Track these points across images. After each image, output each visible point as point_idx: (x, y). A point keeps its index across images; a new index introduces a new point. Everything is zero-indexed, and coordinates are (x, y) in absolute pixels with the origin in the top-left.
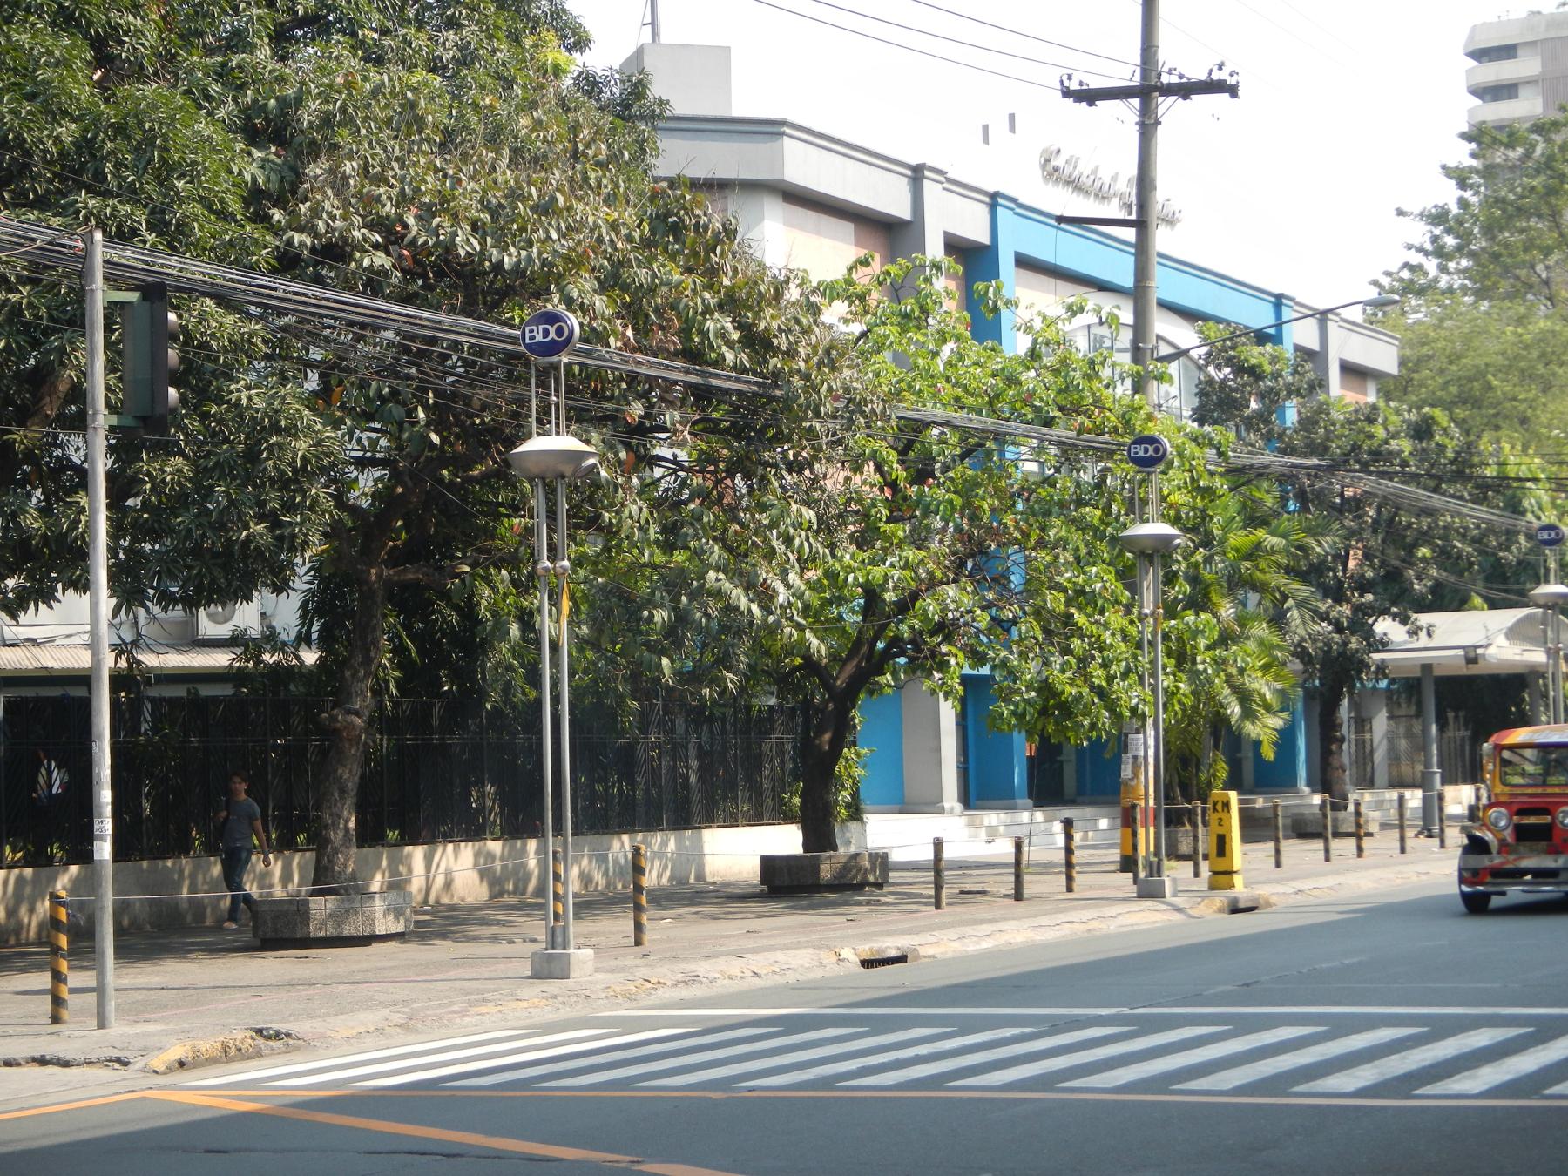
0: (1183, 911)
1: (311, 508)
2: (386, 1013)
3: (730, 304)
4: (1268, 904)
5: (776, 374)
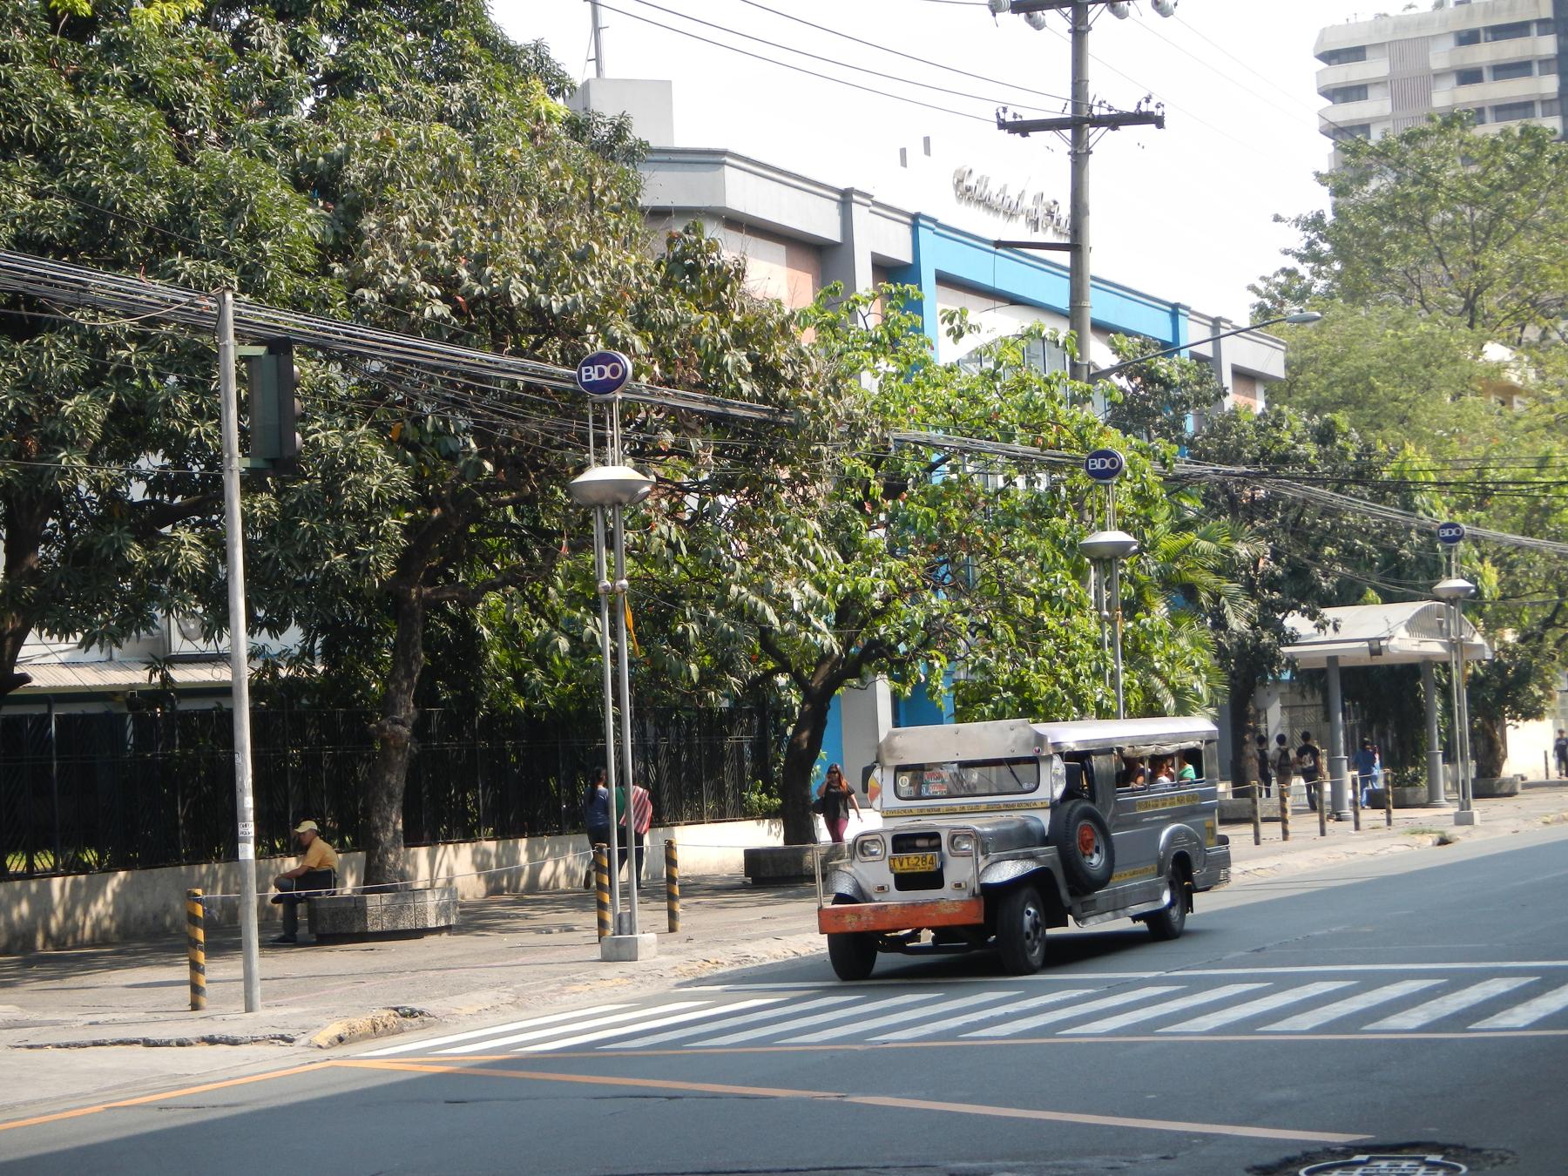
1: (383, 538)
2: (494, 993)
3: (741, 338)
5: (784, 404)
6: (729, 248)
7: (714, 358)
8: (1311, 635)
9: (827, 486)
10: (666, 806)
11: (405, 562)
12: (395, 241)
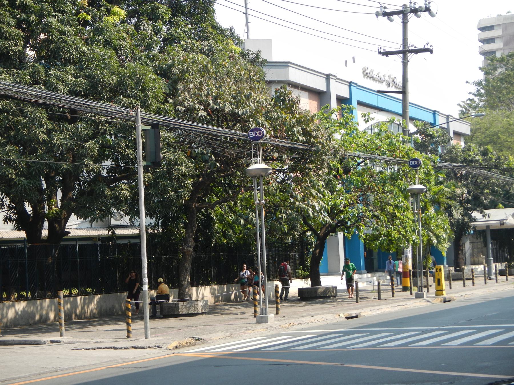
0: (427, 303)
1: (186, 187)
3: (299, 122)
4: (454, 300)
5: (312, 144)
6: (295, 94)
7: (290, 129)
8: (481, 219)
9: (325, 170)
10: (271, 274)
11: (193, 194)
12: (189, 92)
